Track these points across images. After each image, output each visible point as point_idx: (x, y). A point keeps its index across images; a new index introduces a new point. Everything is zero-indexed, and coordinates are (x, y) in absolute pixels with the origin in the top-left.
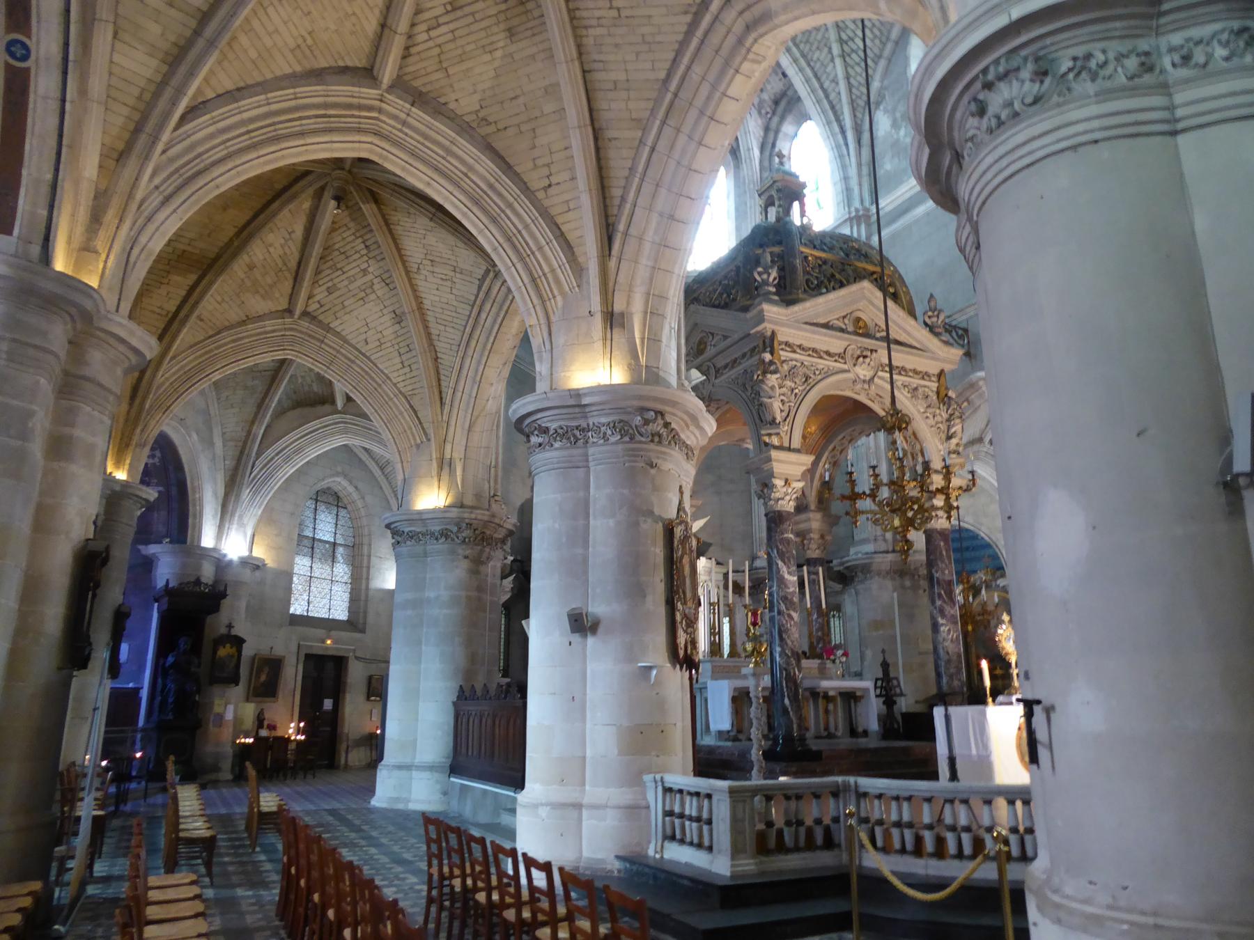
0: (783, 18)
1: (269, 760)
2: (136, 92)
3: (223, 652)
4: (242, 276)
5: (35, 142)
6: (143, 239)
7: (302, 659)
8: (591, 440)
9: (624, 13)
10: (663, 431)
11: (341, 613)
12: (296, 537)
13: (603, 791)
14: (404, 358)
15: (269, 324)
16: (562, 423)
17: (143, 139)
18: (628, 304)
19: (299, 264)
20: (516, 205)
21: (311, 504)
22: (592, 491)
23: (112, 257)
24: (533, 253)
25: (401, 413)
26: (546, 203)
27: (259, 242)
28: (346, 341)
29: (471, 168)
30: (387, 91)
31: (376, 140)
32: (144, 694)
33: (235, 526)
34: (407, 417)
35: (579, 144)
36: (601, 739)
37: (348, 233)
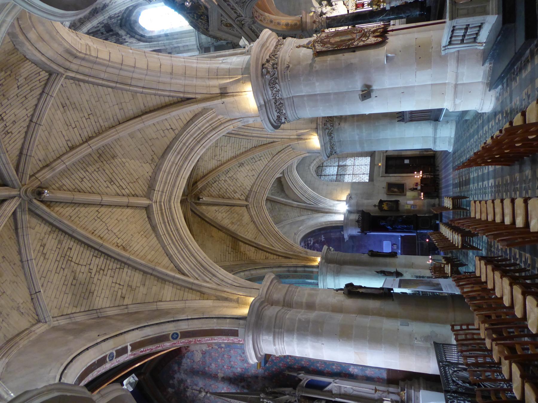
0: (66, 44)
1: (431, 187)
2: (178, 291)
3: (385, 207)
4: (236, 226)
5: (204, 326)
6: (230, 282)
7: (387, 175)
8: (280, 97)
9: (90, 112)
10: (271, 62)
11: (367, 160)
12: (337, 183)
13: (449, 75)
14: (257, 160)
15: (253, 213)
16: (274, 111)
17: (194, 287)
18: (215, 87)
19: (227, 205)
20: (183, 142)
21: (322, 178)
22: (303, 94)
23: (239, 293)
24: (202, 131)
25: (280, 158)
26: (179, 129)
27: (222, 222)
28: (254, 183)
29: (173, 163)
30: (152, 201)
31: (172, 201)
32: (403, 234)
33: (334, 208)
34: (282, 155)
35: (150, 121)
36: (423, 77)
37: (211, 189)
